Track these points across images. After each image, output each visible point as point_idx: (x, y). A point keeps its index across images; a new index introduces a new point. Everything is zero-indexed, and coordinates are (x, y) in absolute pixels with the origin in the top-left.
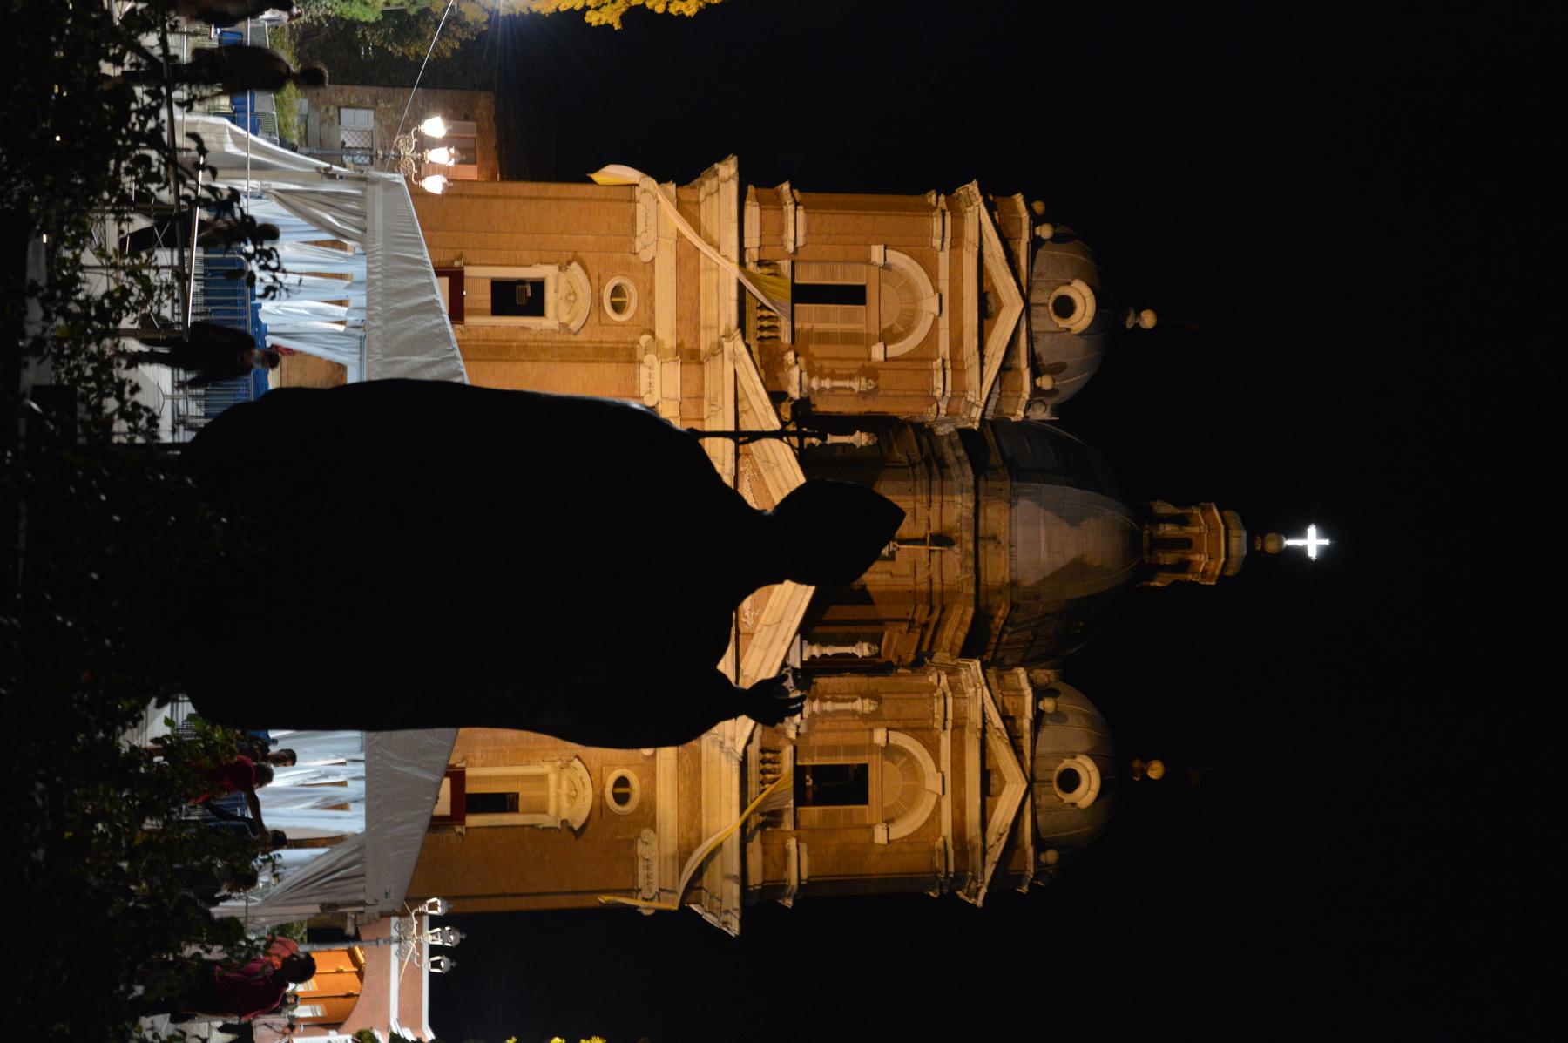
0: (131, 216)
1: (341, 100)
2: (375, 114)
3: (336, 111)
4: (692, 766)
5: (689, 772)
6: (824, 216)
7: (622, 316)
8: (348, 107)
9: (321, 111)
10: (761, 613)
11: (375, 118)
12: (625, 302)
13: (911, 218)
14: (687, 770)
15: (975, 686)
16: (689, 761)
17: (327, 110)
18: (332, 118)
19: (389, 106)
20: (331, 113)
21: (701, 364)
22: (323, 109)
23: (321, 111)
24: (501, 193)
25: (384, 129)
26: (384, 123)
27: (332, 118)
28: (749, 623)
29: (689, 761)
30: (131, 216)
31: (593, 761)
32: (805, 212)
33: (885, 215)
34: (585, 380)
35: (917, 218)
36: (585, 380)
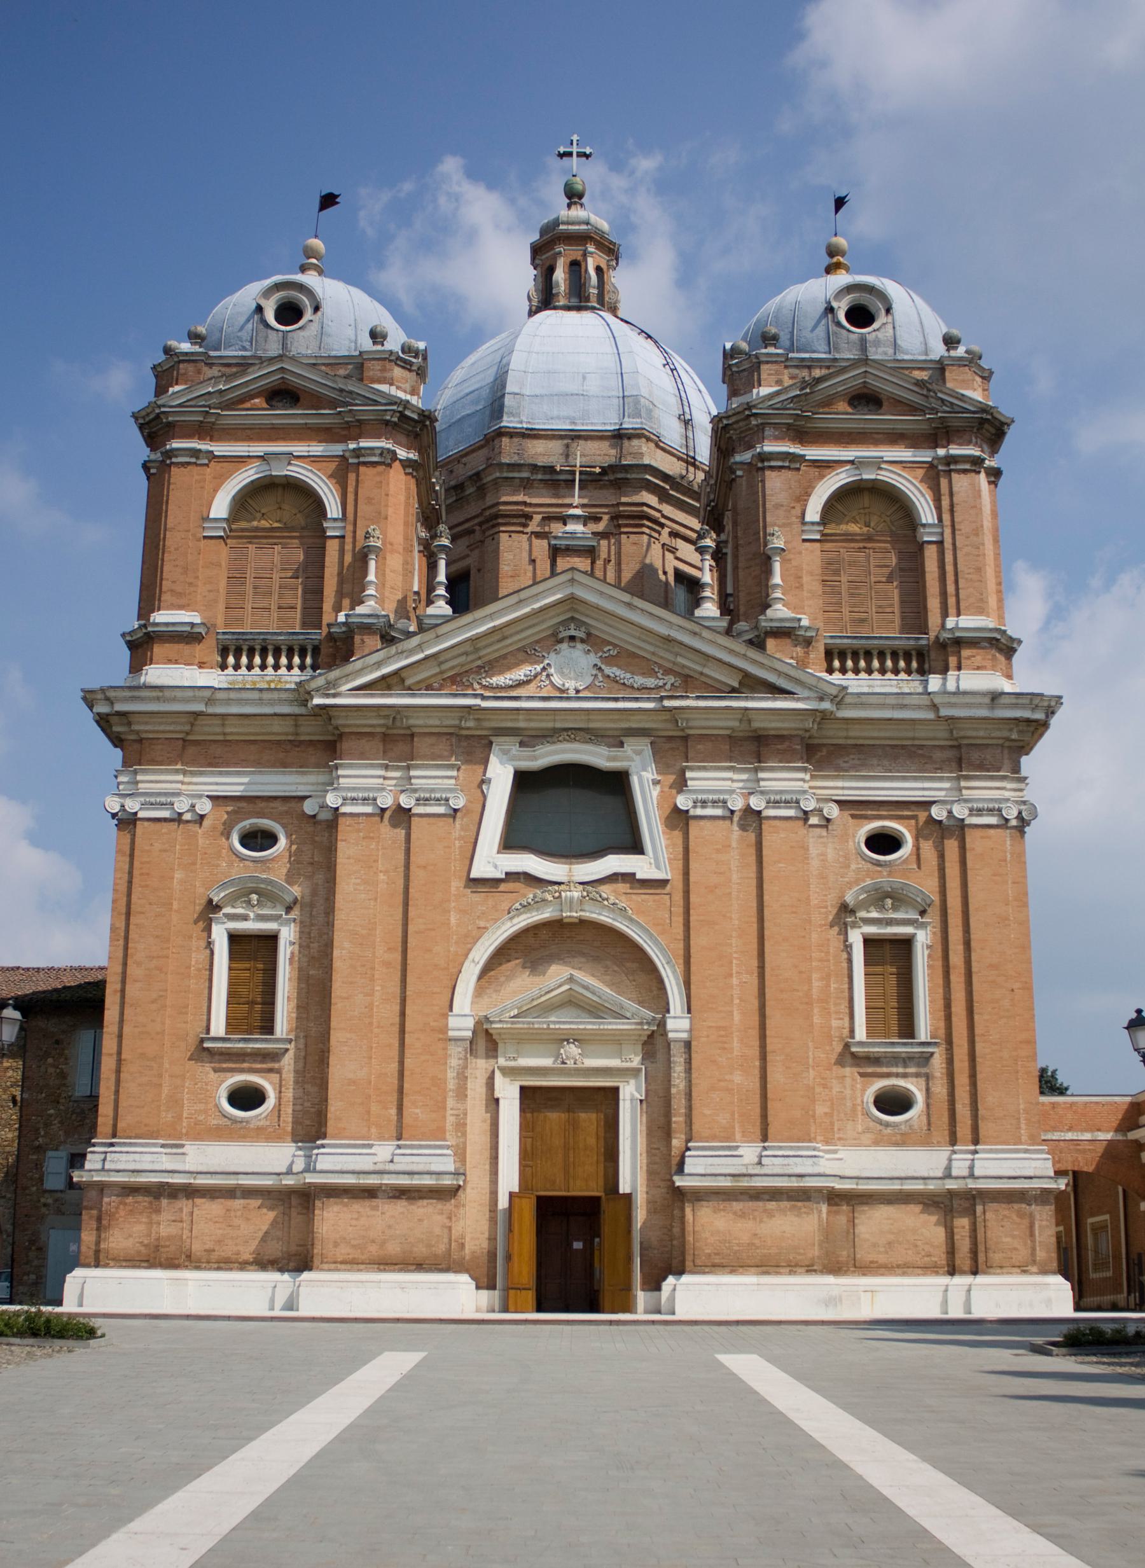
0: (967, 355)
1: (34, 1189)
2: (52, 1150)
3: (46, 1195)
4: (852, 756)
5: (859, 759)
6: (164, 589)
7: (275, 830)
8: (41, 1180)
9: (47, 1212)
10: (660, 666)
11: (57, 1150)
12: (138, 620)
13: (172, 487)
14: (857, 762)
15: (749, 416)
16: (846, 759)
17: (45, 1205)
18: (56, 1200)
19: (42, 1133)
20: (50, 1201)
21: (341, 735)
22: (44, 1210)
23: (47, 1212)
24: (118, 987)
25: (70, 1140)
26: (62, 1138)
27: (56, 1200)
28: (673, 680)
29: (846, 759)
30: (967, 355)
31: (847, 879)
32: (159, 610)
33: (166, 516)
34: (358, 881)
35: (172, 480)
36: (358, 881)
